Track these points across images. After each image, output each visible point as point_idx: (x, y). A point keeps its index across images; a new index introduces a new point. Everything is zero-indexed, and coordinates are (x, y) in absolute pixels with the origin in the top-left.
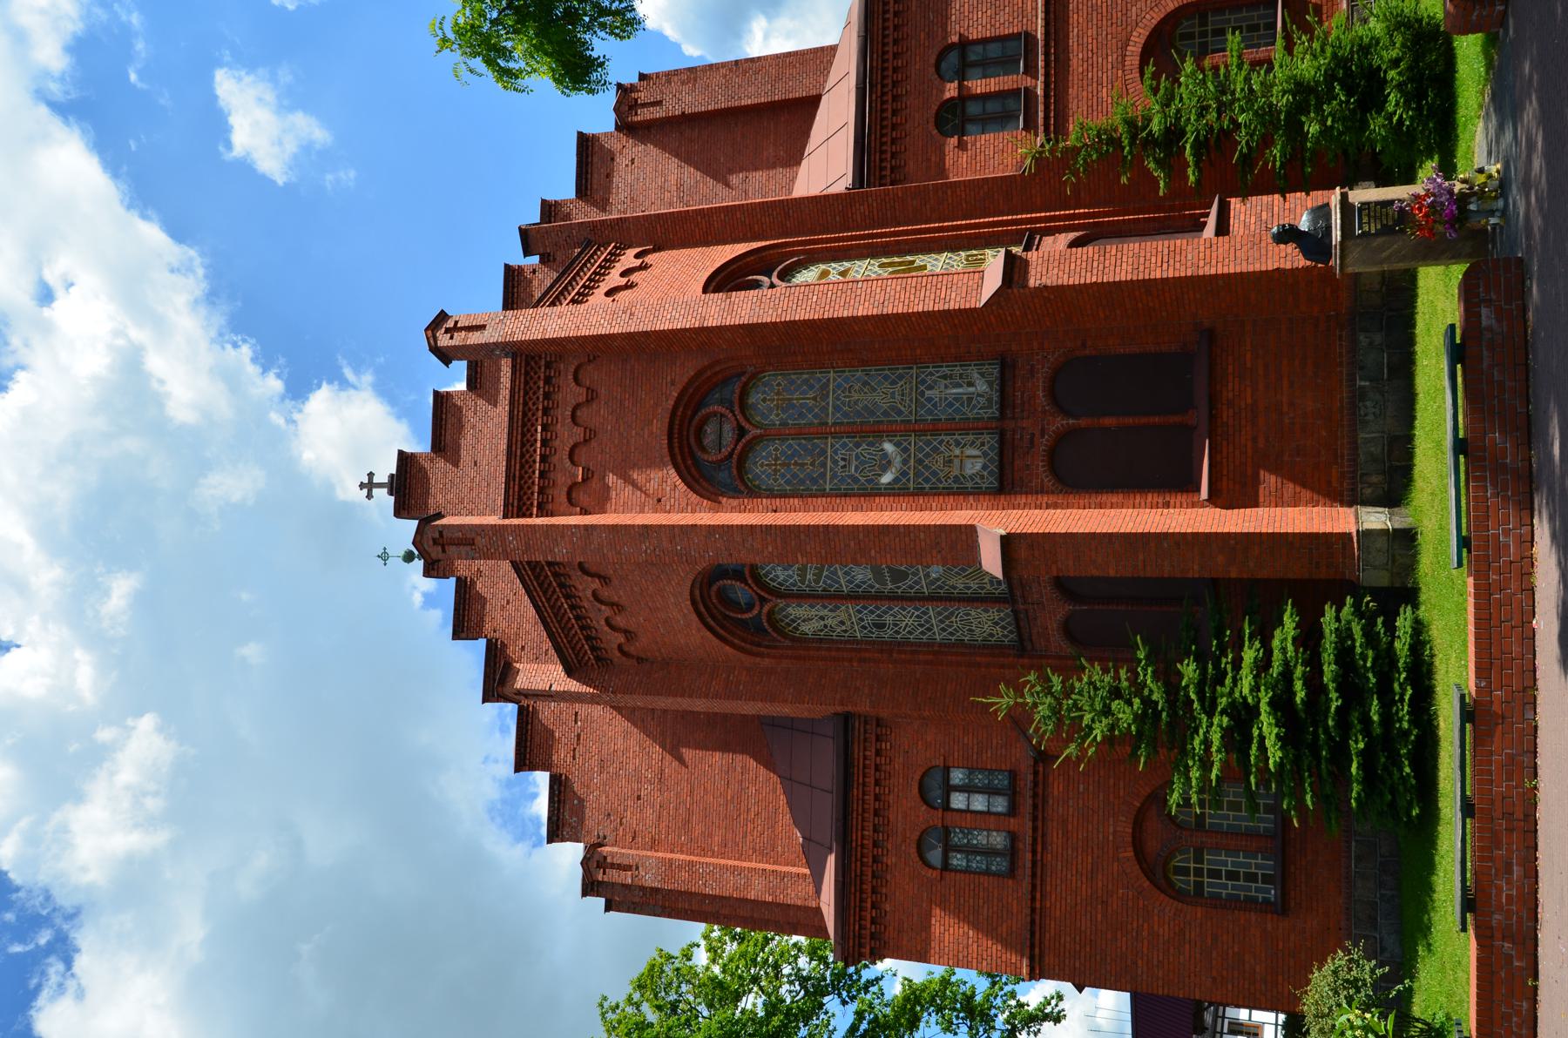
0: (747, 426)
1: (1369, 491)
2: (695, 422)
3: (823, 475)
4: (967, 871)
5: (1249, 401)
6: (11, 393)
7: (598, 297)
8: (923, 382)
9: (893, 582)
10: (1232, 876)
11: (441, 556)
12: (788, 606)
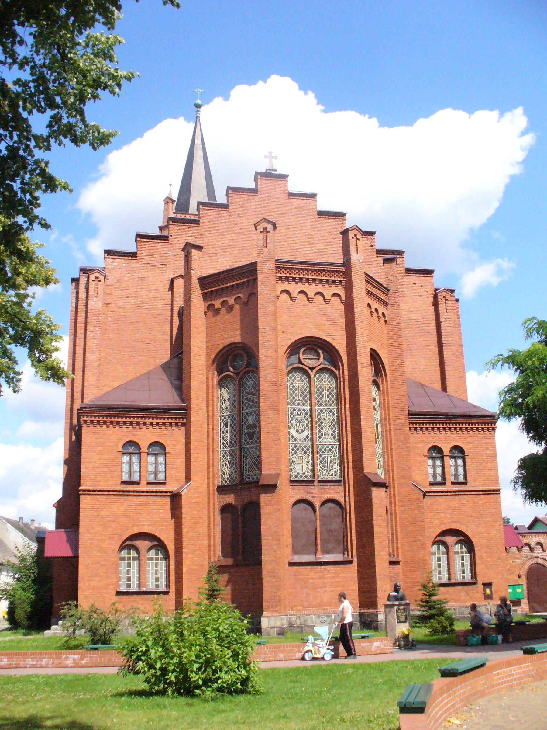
1: (294, 619)
2: (315, 347)
3: (294, 404)
4: (122, 463)
5: (326, 576)
6: (516, 465)
7: (368, 300)
8: (332, 447)
9: (248, 433)
11: (259, 231)
12: (234, 385)
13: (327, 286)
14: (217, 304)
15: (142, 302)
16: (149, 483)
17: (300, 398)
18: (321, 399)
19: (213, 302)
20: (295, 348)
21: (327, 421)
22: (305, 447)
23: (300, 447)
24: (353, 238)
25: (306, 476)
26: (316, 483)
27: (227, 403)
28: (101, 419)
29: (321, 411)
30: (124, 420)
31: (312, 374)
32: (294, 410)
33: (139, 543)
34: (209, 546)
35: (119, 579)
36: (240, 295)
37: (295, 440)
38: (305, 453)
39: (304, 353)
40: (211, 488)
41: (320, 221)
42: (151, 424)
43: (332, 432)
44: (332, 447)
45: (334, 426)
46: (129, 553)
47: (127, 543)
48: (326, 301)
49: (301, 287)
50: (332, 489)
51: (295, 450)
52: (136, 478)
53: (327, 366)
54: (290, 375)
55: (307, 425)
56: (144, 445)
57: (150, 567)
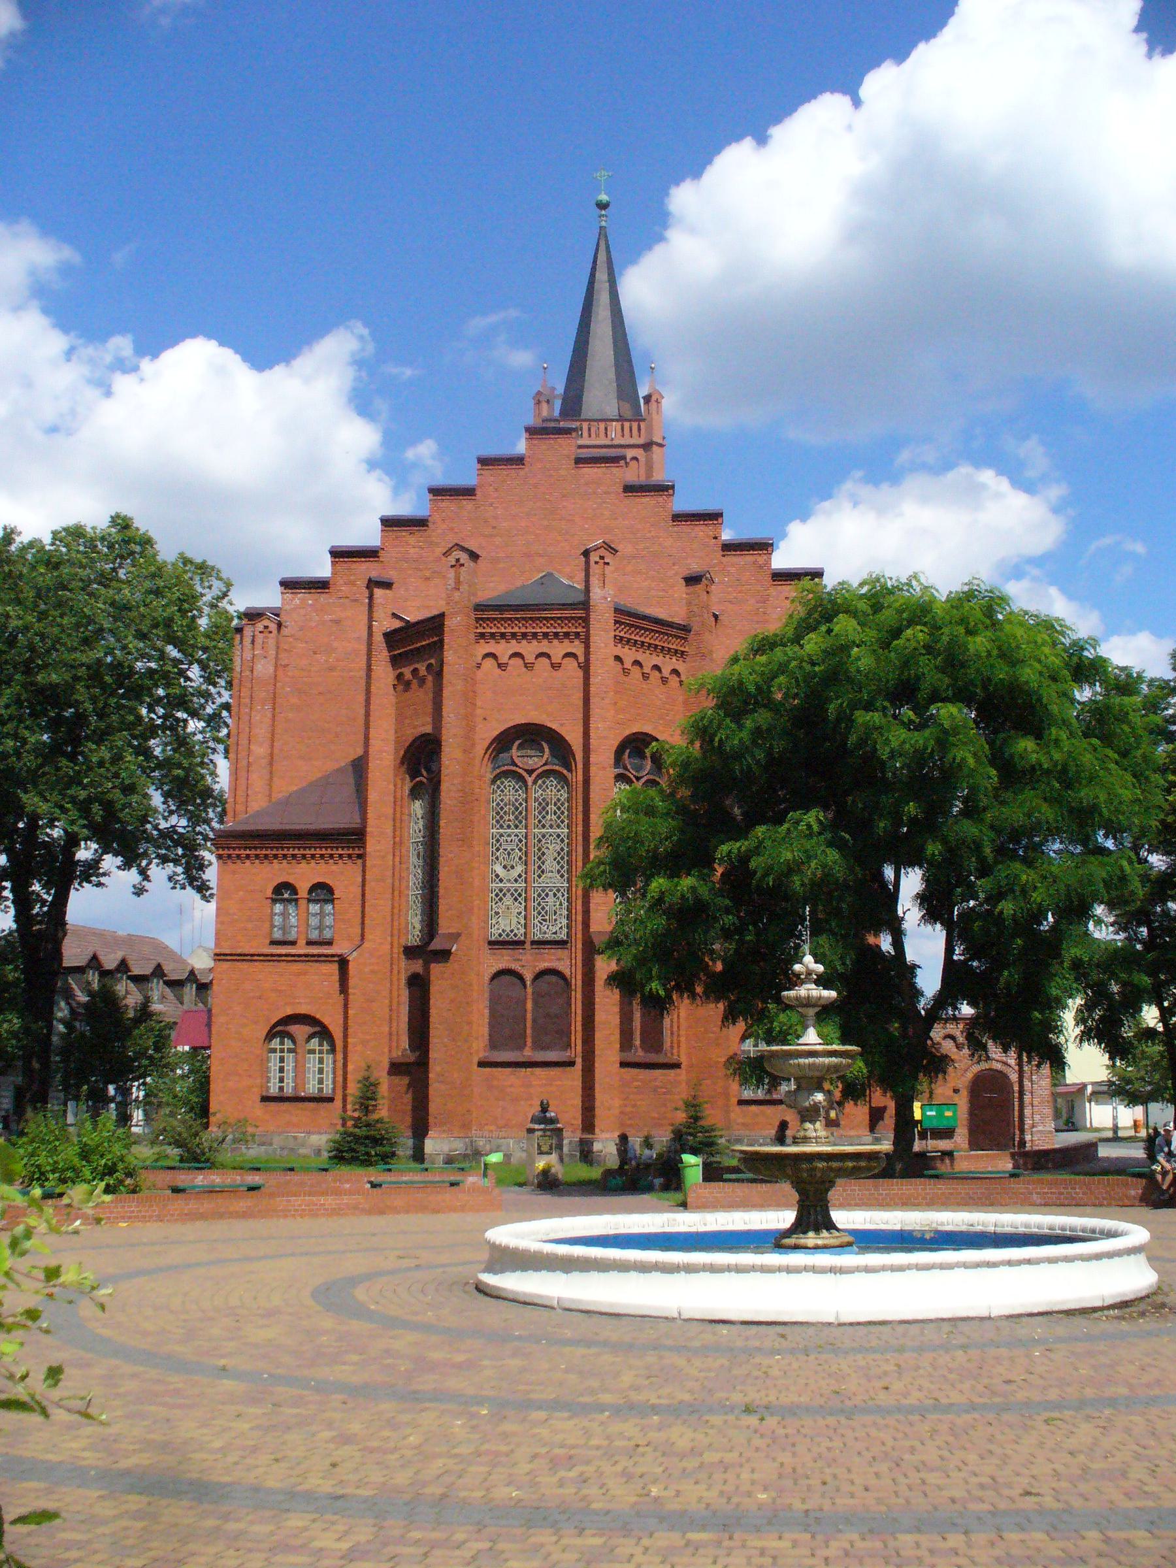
0: (534, 775)
3: (502, 827)
4: (273, 914)
8: (558, 891)
10: (282, 1070)
13: (556, 642)
14: (408, 675)
15: (338, 660)
16: (310, 943)
17: (512, 817)
18: (544, 817)
19: (417, 666)
20: (502, 742)
21: (551, 851)
22: (516, 890)
23: (509, 890)
24: (596, 563)
25: (515, 935)
26: (528, 946)
27: (421, 822)
28: (242, 852)
29: (544, 836)
30: (274, 852)
31: (530, 780)
32: (501, 835)
33: (294, 1029)
34: (390, 1034)
35: (268, 1080)
36: (432, 661)
37: (501, 881)
38: (516, 899)
39: (520, 747)
40: (395, 950)
41: (627, 501)
42: (313, 856)
43: (558, 867)
44: (558, 891)
45: (562, 858)
46: (282, 1043)
47: (279, 1028)
48: (555, 666)
49: (514, 647)
50: (554, 954)
51: (500, 895)
52: (292, 936)
53: (557, 768)
54: (540, 782)
55: (520, 858)
56: (303, 889)
57: (312, 1062)
